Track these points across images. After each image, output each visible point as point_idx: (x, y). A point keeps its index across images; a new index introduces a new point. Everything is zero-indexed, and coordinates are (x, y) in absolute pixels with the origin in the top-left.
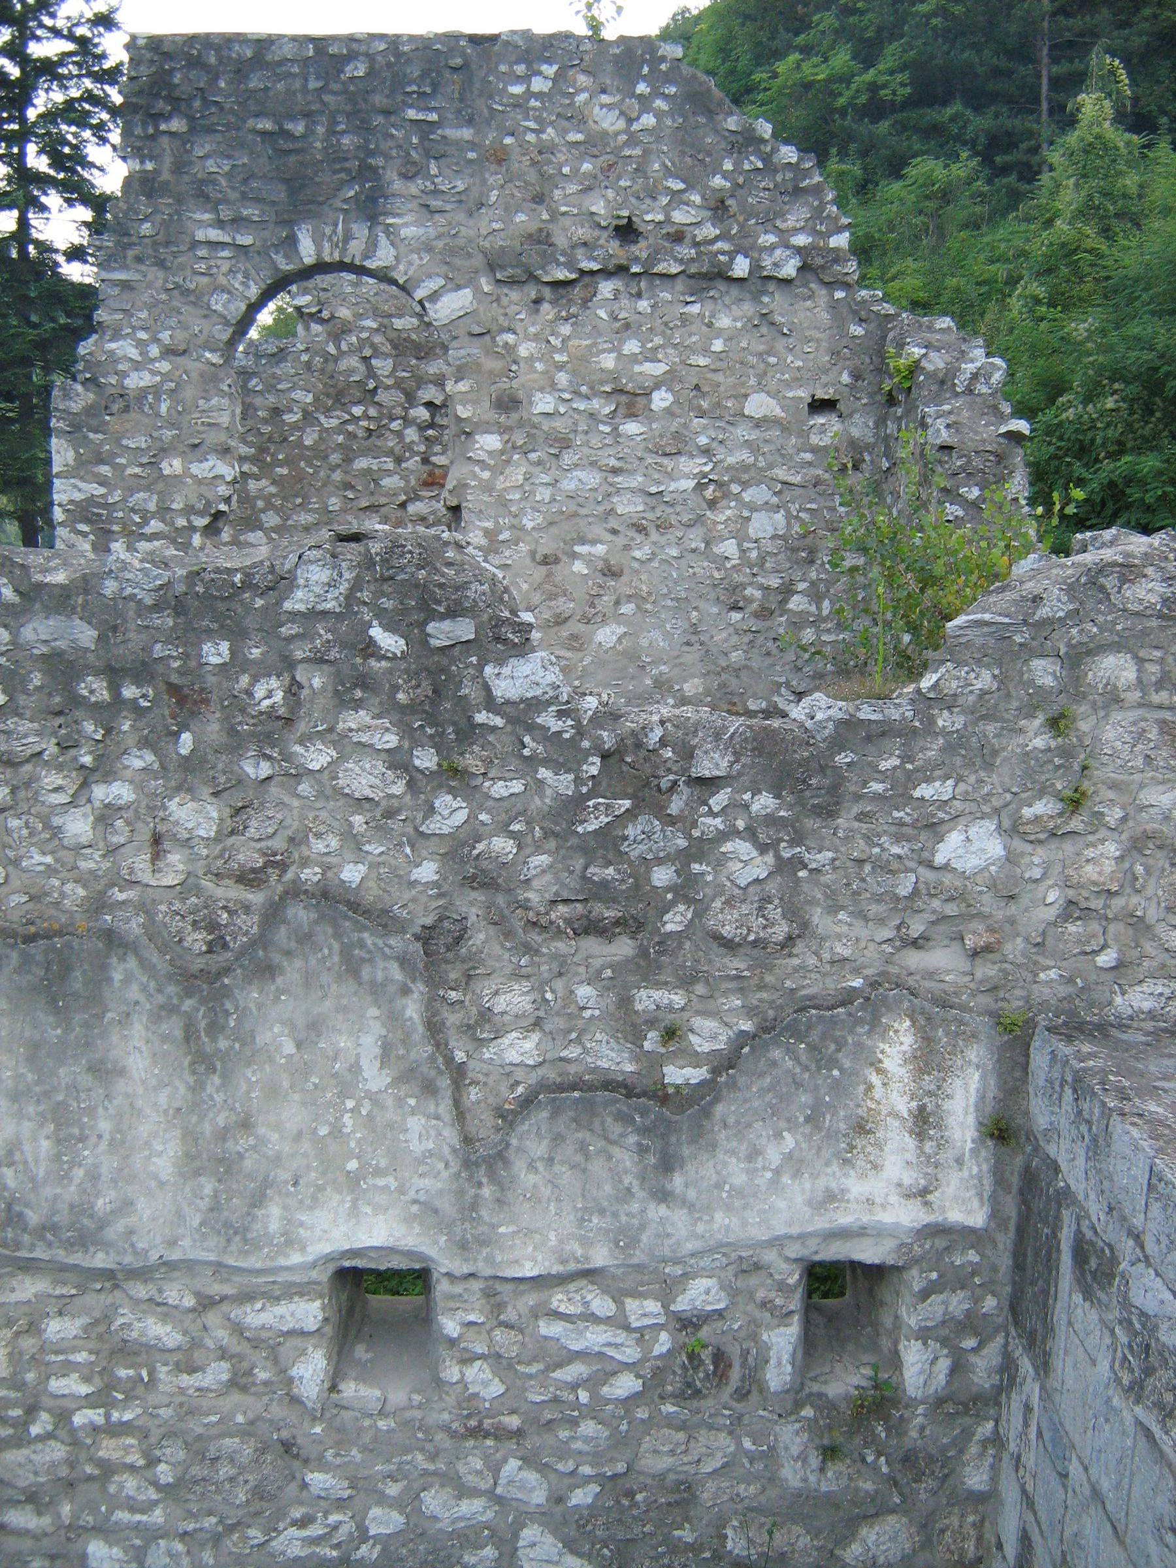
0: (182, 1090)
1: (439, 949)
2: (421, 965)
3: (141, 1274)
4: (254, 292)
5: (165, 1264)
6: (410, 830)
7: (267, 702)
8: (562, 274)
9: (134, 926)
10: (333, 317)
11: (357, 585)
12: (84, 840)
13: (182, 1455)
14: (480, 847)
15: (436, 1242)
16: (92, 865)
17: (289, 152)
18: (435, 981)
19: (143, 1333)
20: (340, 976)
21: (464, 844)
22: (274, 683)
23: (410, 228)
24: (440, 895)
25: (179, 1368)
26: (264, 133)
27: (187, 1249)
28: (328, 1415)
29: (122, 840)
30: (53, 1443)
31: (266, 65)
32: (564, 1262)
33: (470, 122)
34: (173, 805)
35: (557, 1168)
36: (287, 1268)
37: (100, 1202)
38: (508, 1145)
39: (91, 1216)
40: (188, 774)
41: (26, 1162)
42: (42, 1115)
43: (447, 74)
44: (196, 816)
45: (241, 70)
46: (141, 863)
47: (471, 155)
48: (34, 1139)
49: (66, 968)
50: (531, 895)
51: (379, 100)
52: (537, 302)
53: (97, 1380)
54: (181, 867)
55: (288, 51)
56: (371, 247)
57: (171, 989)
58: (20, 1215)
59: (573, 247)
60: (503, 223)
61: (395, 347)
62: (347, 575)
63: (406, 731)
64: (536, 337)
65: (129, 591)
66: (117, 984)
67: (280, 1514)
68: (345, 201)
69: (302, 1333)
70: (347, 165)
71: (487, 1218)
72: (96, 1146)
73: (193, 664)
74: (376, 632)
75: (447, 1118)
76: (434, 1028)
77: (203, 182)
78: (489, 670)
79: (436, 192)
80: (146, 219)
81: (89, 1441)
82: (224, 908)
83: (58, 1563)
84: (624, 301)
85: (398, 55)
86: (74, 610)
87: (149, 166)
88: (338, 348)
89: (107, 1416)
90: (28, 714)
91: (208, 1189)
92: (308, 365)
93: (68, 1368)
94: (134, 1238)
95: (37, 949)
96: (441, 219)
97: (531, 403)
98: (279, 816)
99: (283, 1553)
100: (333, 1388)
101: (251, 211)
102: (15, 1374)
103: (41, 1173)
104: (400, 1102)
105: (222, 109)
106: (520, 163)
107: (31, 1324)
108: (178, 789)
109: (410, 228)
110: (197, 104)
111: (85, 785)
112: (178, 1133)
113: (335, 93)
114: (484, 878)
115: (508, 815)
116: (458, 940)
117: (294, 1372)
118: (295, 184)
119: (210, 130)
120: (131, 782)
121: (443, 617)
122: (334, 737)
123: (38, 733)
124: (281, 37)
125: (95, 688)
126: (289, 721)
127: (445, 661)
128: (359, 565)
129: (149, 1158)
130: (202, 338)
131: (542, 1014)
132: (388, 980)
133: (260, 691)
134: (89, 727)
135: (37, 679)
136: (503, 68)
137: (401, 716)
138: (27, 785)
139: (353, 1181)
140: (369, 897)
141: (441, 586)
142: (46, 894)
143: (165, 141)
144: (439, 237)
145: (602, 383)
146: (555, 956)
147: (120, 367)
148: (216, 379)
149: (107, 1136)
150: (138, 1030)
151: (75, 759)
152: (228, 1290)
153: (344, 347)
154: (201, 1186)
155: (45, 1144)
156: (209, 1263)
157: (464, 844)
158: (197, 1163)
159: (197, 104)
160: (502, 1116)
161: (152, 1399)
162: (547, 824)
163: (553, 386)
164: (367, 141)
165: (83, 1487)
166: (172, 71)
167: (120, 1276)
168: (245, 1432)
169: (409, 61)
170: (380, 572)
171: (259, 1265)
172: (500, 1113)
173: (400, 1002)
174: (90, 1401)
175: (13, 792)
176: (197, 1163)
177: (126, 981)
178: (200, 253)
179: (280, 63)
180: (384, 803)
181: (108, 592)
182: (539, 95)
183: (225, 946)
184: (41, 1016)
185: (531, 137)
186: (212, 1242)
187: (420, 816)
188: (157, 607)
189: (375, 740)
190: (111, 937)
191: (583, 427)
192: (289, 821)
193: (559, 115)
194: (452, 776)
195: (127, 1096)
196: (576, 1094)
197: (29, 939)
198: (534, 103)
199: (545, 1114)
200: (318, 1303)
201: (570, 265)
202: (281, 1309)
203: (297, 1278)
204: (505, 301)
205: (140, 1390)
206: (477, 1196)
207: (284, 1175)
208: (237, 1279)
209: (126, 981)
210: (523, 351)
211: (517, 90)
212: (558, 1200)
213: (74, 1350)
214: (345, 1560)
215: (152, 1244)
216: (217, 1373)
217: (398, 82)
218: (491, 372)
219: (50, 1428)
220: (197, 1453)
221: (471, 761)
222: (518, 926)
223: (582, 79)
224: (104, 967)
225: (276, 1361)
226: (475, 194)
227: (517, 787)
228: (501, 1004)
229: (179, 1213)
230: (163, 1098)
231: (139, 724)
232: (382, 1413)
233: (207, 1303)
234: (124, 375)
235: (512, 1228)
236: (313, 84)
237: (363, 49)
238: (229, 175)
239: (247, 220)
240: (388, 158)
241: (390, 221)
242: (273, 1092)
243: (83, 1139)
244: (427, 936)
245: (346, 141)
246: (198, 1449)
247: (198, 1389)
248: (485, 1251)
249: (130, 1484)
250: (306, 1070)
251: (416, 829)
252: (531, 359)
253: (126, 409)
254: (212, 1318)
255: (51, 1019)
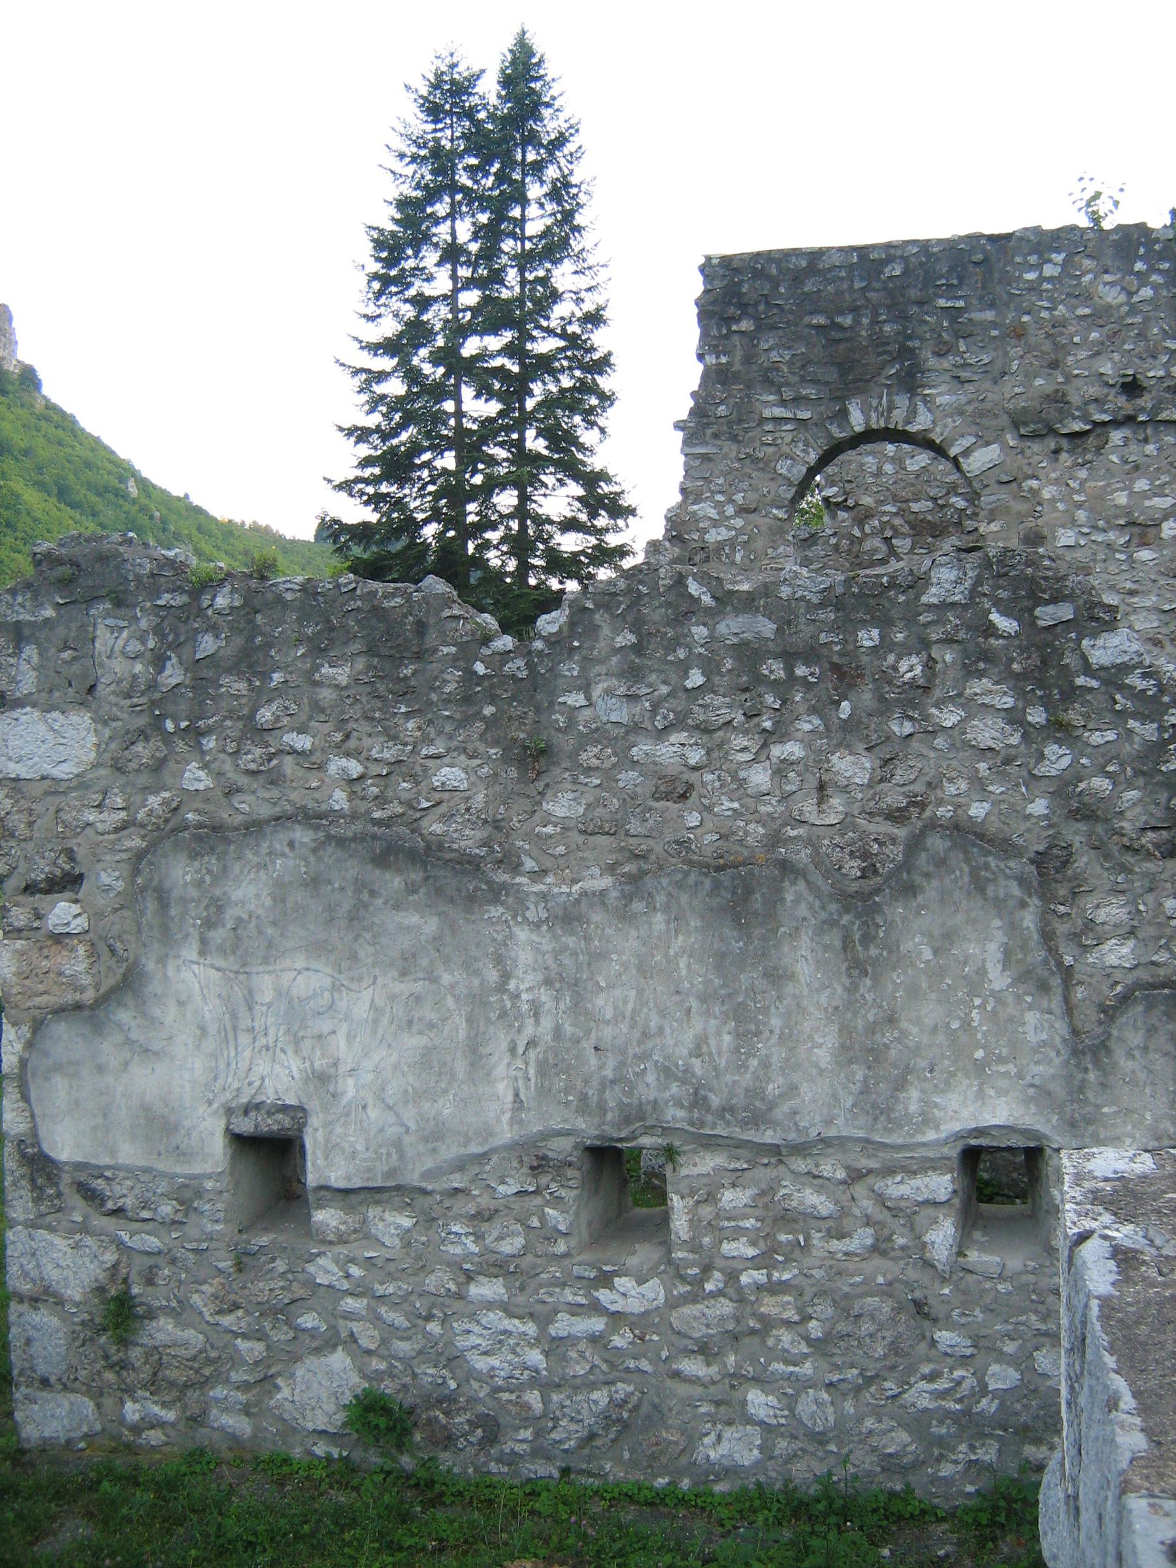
0: (840, 990)
1: (1050, 869)
2: (1035, 883)
3: (800, 1149)
4: (813, 457)
5: (822, 1140)
6: (1025, 773)
7: (909, 675)
8: (1077, 426)
9: (803, 856)
10: (857, 505)
11: (978, 582)
12: (764, 789)
13: (830, 1311)
14: (1082, 786)
15: (1049, 1121)
16: (770, 809)
17: (838, 341)
18: (1047, 897)
19: (801, 1203)
20: (969, 893)
21: (1068, 784)
22: (914, 660)
23: (944, 396)
24: (1050, 826)
25: (830, 1235)
26: (818, 327)
27: (842, 1127)
28: (955, 1278)
29: (794, 788)
30: (722, 1299)
31: (818, 272)
32: (1159, 1139)
33: (992, 305)
34: (835, 759)
35: (1154, 1056)
36: (923, 1145)
37: (770, 1087)
38: (1110, 1035)
39: (763, 1099)
40: (847, 734)
41: (710, 1054)
42: (725, 1013)
43: (970, 268)
44: (852, 767)
45: (798, 278)
46: (808, 807)
47: (994, 333)
48: (719, 1034)
49: (749, 891)
50: (1124, 824)
51: (913, 293)
52: (1057, 452)
53: (762, 1244)
54: (841, 808)
55: (836, 260)
56: (912, 413)
57: (833, 907)
58: (705, 1098)
59: (1086, 404)
60: (1026, 387)
61: (913, 528)
62: (970, 574)
63: (1021, 694)
64: (1056, 482)
65: (800, 594)
66: (788, 904)
67: (911, 1369)
68: (888, 378)
69: (936, 1204)
70: (889, 348)
71: (1092, 1100)
72: (768, 1040)
73: (851, 647)
74: (995, 617)
75: (1058, 1011)
76: (1047, 936)
77: (769, 369)
78: (1085, 643)
79: (966, 365)
80: (722, 402)
81: (753, 1298)
82: (875, 840)
83: (722, 1408)
84: (1133, 447)
85: (928, 254)
86: (757, 610)
87: (724, 360)
88: (863, 531)
89: (769, 1276)
90: (722, 691)
91: (859, 1076)
92: (836, 547)
93: (739, 1232)
94: (798, 1118)
95: (725, 877)
96: (970, 388)
97: (1055, 538)
98: (919, 765)
99: (913, 1405)
100: (960, 1253)
101: (809, 391)
102: (693, 1238)
103: (723, 1064)
104: (1019, 999)
105: (782, 310)
106: (1036, 337)
107: (709, 1194)
108: (839, 745)
109: (944, 396)
110: (762, 308)
111: (765, 745)
112: (835, 1027)
113: (877, 291)
114: (1086, 812)
115: (1104, 757)
116: (1066, 863)
117: (927, 1238)
118: (845, 367)
119: (774, 327)
120: (801, 741)
121: (1047, 603)
122: (963, 700)
123: (730, 706)
124: (829, 249)
125: (775, 669)
126: (926, 689)
127: (1049, 638)
128: (979, 566)
129: (811, 1049)
130: (770, 497)
131: (1135, 923)
132: (1009, 896)
133: (903, 666)
134: (769, 699)
135: (729, 664)
136: (1018, 259)
137: (1016, 681)
138: (720, 746)
139: (980, 1068)
140: (994, 827)
141: (1046, 578)
142: (733, 833)
143: (736, 339)
144: (969, 403)
145: (1117, 517)
146: (1145, 875)
147: (701, 525)
148: (782, 532)
149: (777, 1031)
150: (805, 941)
151: (758, 725)
152: (873, 1164)
153: (868, 530)
154: (853, 1073)
155: (727, 1038)
156: (858, 1140)
157: (1068, 784)
158: (851, 1054)
159: (762, 308)
160: (1104, 1012)
161: (807, 1261)
162: (1137, 765)
163: (1073, 523)
164: (905, 328)
165: (746, 1340)
166: (741, 282)
167: (784, 1151)
168: (886, 1291)
169: (937, 260)
170: (998, 569)
171: (900, 1141)
172: (1103, 1009)
173: (1019, 914)
174: (755, 1263)
175: (707, 754)
176: (851, 1054)
177: (797, 901)
178: (767, 428)
179: (830, 270)
180: (1003, 752)
181: (783, 595)
182: (1050, 280)
183: (876, 872)
184: (726, 930)
185: (1045, 314)
186: (861, 1121)
187: (1032, 761)
188: (822, 605)
189: (995, 702)
190: (785, 866)
191: (1101, 556)
192: (927, 770)
193: (1068, 294)
194: (1059, 730)
195: (795, 997)
196: (1166, 991)
197: (718, 869)
198: (1046, 286)
199: (1140, 1008)
200: (948, 1177)
201: (1085, 418)
202: (917, 1182)
203: (931, 1154)
204: (1028, 453)
205: (797, 1252)
206: (1083, 1080)
207: (922, 1063)
208: (881, 1154)
209: (797, 901)
210: (1046, 494)
211: (1031, 276)
212: (1153, 1084)
213: (745, 1217)
214: (967, 1412)
215: (813, 1126)
216: (863, 1238)
217: (929, 278)
218: (1019, 513)
219: (721, 1285)
220: (843, 1310)
221: (1074, 716)
222: (1115, 849)
223: (1087, 263)
224: (779, 890)
225: (912, 1229)
226: (998, 366)
227: (1111, 736)
228: (1101, 915)
229: (835, 1096)
230: (823, 999)
231: (809, 696)
232: (1001, 1277)
233: (856, 1176)
234: (705, 531)
235: (1114, 1109)
236: (858, 285)
237: (899, 253)
238: (790, 363)
239: (806, 398)
240: (922, 339)
241: (927, 392)
242: (914, 992)
243: (758, 1033)
244: (1040, 860)
245: (887, 328)
246: (845, 1307)
247: (846, 1254)
248: (1091, 1128)
249: (786, 1338)
250: (941, 972)
251: (1030, 773)
252: (1053, 500)
253: (707, 560)
254: (859, 1190)
255: (735, 933)
